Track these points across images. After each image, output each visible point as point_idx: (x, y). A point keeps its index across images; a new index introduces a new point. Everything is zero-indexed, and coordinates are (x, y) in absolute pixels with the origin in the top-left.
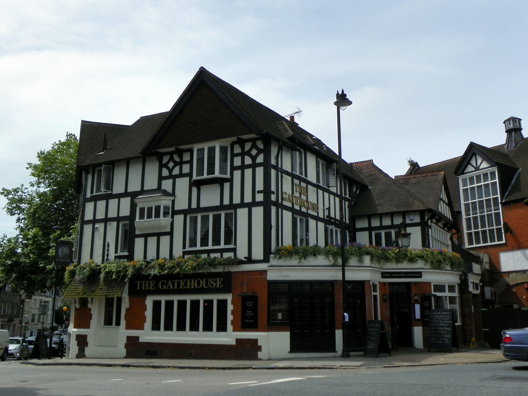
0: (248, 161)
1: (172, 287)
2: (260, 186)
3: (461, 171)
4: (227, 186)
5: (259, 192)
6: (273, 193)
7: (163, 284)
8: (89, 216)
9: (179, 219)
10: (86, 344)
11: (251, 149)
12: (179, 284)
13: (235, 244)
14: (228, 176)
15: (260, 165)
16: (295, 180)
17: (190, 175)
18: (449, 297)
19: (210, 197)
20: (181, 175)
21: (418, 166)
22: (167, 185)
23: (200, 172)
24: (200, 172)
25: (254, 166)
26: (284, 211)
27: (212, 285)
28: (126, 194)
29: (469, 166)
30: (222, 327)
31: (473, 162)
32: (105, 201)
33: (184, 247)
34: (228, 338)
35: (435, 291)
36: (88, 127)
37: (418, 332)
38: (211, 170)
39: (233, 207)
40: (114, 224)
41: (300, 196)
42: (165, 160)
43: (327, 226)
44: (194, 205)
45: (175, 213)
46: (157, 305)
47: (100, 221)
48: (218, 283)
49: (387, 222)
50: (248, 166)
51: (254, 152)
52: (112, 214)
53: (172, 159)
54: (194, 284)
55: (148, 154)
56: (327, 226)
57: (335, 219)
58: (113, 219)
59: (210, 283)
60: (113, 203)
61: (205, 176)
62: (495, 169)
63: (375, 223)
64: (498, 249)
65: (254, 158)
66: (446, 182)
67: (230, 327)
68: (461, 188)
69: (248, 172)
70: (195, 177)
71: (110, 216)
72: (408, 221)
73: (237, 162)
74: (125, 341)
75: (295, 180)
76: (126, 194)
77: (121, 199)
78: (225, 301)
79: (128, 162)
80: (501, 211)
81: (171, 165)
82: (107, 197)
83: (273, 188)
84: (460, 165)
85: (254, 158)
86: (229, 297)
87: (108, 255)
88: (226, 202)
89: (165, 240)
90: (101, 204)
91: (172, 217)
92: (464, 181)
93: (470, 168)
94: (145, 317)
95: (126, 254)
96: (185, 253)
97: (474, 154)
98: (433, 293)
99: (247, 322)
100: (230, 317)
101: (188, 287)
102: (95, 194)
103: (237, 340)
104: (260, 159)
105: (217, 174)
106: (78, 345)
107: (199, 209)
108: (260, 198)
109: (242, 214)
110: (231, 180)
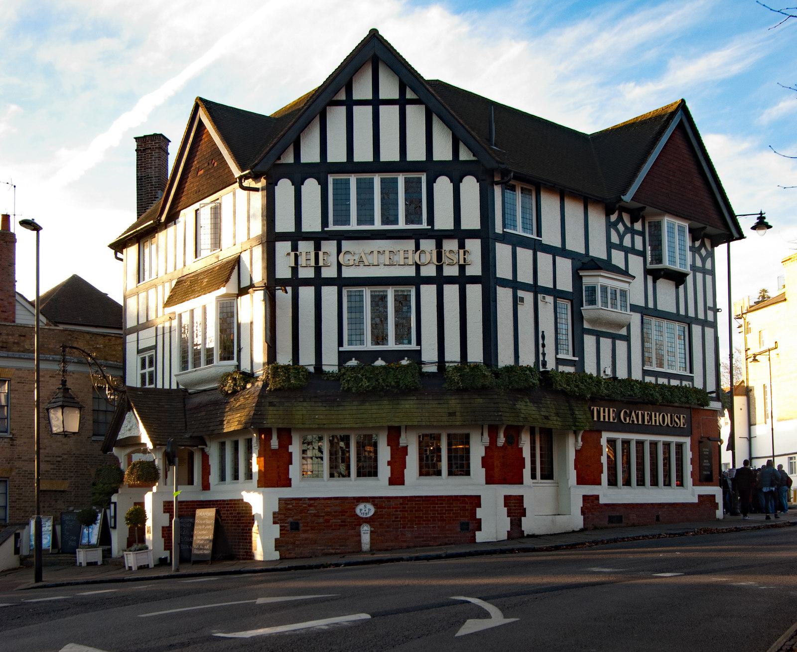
1: (636, 422)
10: (523, 513)
26: (642, 304)
27: (677, 424)
43: (430, 227)
56: (430, 227)
59: (675, 421)
67: (688, 480)
74: (580, 504)
94: (691, 451)
100: (688, 468)
101: (653, 424)
103: (700, 496)
106: (509, 514)
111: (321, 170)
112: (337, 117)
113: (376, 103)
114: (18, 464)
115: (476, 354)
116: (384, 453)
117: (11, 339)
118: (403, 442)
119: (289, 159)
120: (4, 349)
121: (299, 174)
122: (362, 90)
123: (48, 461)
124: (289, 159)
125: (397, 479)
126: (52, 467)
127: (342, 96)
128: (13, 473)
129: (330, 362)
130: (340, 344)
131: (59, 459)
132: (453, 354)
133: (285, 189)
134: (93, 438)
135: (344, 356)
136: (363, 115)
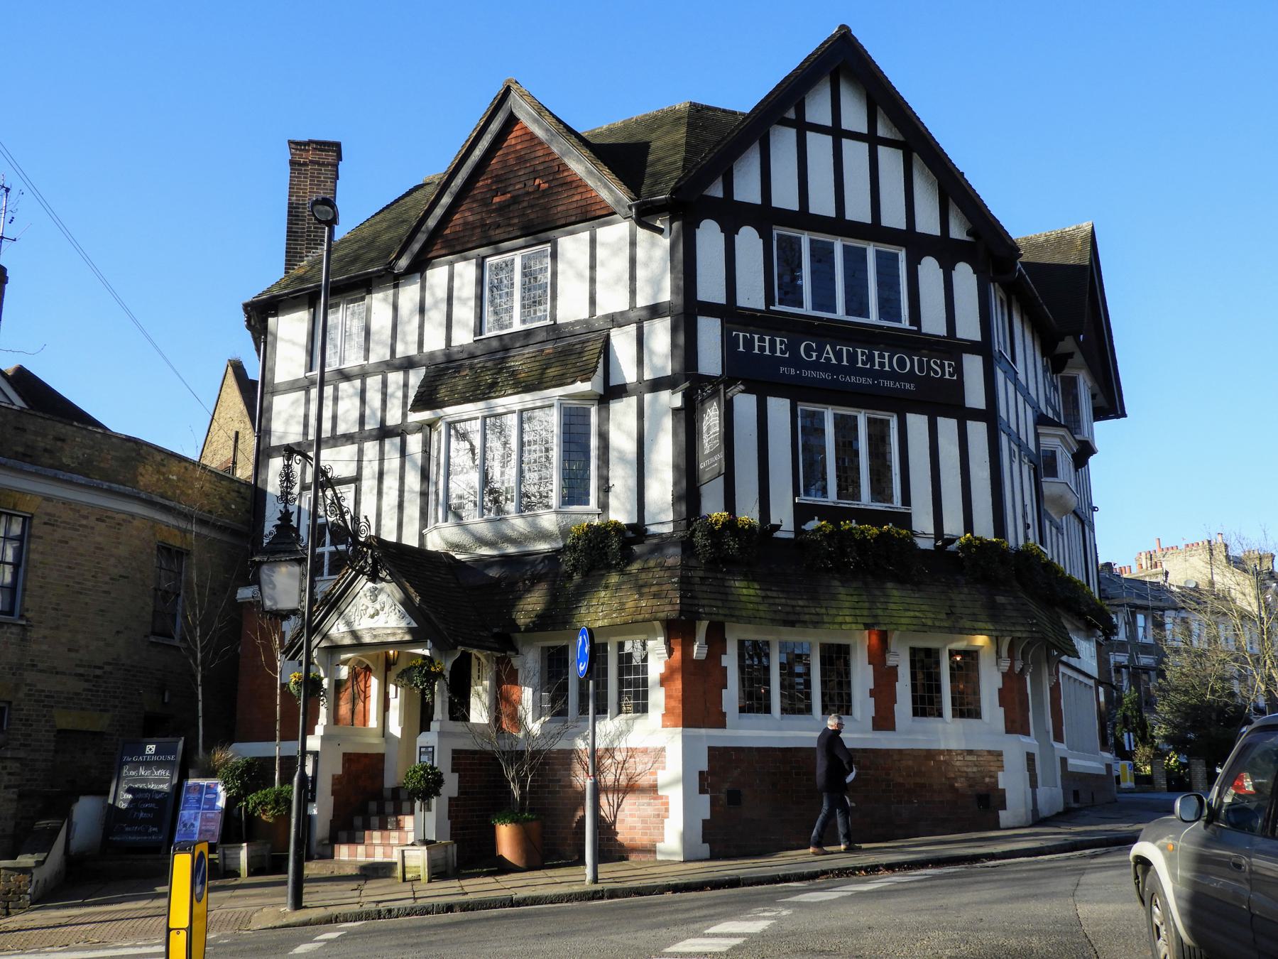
111: (764, 216)
112: (783, 142)
113: (837, 133)
114: (30, 676)
115: (984, 528)
116: (862, 677)
117: (41, 444)
118: (891, 661)
119: (717, 191)
120: (28, 459)
121: (733, 216)
122: (818, 110)
123: (82, 675)
124: (717, 191)
125: (884, 721)
126: (86, 685)
127: (791, 114)
128: (21, 695)
129: (783, 515)
130: (796, 493)
131: (98, 672)
132: (954, 525)
133: (709, 236)
134: (153, 639)
135: (802, 513)
136: (820, 146)
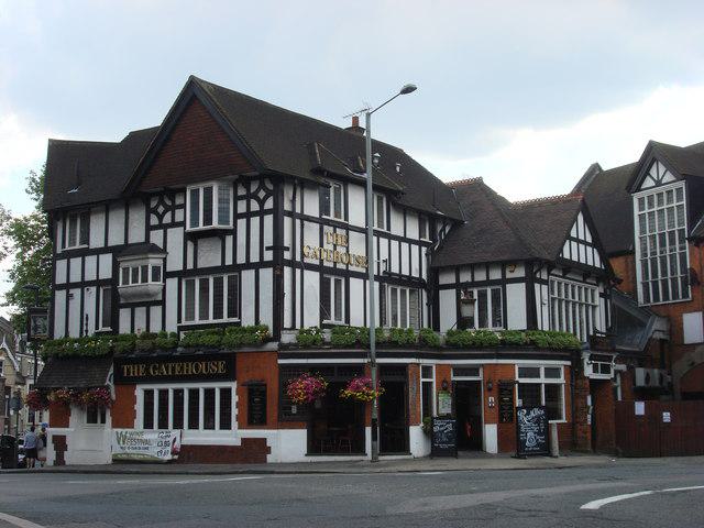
0: (255, 206)
2: (269, 241)
3: (634, 188)
4: (229, 240)
5: (268, 248)
6: (288, 249)
7: (154, 368)
8: (61, 279)
9: (172, 283)
11: (258, 191)
12: (173, 369)
13: (240, 318)
14: (231, 226)
15: (268, 212)
16: (325, 227)
17: (183, 224)
18: (546, 385)
19: (209, 257)
20: (174, 224)
21: (600, 169)
22: (156, 238)
23: (195, 222)
24: (195, 222)
25: (262, 213)
28: (106, 250)
29: (648, 178)
30: (226, 425)
31: (653, 172)
32: (109, 245)
33: (179, 320)
34: (233, 437)
35: (520, 377)
36: (196, 99)
37: (491, 433)
38: (208, 220)
39: (237, 268)
40: (94, 289)
41: (335, 249)
42: (153, 204)
44: (190, 266)
45: (168, 275)
46: (148, 394)
47: (75, 285)
48: (220, 367)
49: (480, 276)
50: (255, 214)
51: (262, 194)
52: (90, 276)
53: (161, 202)
54: (191, 369)
55: (129, 197)
57: (400, 275)
58: (91, 283)
60: (91, 260)
61: (201, 227)
62: (682, 184)
63: (465, 277)
64: (110, 469)
65: (262, 203)
66: (587, 208)
68: (636, 212)
69: (255, 221)
70: (188, 228)
71: (72, 280)
72: (509, 275)
73: (242, 207)
75: (325, 227)
76: (106, 250)
77: (86, 258)
78: (229, 390)
79: (107, 207)
80: (687, 250)
81: (161, 209)
82: (83, 253)
83: (287, 242)
84: (634, 176)
85: (262, 203)
86: (233, 386)
87: (87, 331)
88: (229, 262)
89: (156, 311)
90: (76, 262)
91: (164, 281)
92: (641, 201)
93: (649, 182)
95: (109, 329)
96: (180, 329)
97: (654, 160)
98: (517, 379)
99: (255, 417)
100: (234, 411)
102: (67, 248)
104: (269, 204)
105: (215, 224)
107: (196, 271)
108: (269, 256)
109: (248, 277)
110: (234, 232)
